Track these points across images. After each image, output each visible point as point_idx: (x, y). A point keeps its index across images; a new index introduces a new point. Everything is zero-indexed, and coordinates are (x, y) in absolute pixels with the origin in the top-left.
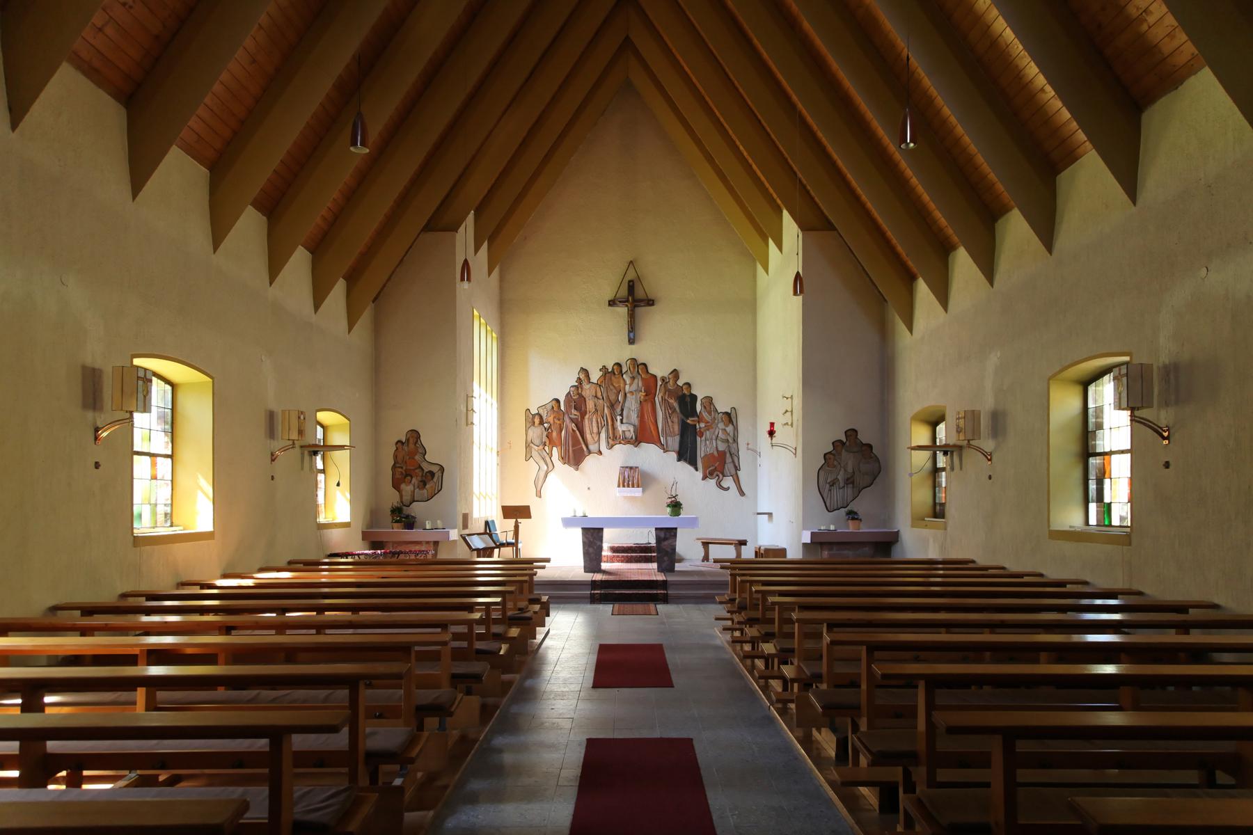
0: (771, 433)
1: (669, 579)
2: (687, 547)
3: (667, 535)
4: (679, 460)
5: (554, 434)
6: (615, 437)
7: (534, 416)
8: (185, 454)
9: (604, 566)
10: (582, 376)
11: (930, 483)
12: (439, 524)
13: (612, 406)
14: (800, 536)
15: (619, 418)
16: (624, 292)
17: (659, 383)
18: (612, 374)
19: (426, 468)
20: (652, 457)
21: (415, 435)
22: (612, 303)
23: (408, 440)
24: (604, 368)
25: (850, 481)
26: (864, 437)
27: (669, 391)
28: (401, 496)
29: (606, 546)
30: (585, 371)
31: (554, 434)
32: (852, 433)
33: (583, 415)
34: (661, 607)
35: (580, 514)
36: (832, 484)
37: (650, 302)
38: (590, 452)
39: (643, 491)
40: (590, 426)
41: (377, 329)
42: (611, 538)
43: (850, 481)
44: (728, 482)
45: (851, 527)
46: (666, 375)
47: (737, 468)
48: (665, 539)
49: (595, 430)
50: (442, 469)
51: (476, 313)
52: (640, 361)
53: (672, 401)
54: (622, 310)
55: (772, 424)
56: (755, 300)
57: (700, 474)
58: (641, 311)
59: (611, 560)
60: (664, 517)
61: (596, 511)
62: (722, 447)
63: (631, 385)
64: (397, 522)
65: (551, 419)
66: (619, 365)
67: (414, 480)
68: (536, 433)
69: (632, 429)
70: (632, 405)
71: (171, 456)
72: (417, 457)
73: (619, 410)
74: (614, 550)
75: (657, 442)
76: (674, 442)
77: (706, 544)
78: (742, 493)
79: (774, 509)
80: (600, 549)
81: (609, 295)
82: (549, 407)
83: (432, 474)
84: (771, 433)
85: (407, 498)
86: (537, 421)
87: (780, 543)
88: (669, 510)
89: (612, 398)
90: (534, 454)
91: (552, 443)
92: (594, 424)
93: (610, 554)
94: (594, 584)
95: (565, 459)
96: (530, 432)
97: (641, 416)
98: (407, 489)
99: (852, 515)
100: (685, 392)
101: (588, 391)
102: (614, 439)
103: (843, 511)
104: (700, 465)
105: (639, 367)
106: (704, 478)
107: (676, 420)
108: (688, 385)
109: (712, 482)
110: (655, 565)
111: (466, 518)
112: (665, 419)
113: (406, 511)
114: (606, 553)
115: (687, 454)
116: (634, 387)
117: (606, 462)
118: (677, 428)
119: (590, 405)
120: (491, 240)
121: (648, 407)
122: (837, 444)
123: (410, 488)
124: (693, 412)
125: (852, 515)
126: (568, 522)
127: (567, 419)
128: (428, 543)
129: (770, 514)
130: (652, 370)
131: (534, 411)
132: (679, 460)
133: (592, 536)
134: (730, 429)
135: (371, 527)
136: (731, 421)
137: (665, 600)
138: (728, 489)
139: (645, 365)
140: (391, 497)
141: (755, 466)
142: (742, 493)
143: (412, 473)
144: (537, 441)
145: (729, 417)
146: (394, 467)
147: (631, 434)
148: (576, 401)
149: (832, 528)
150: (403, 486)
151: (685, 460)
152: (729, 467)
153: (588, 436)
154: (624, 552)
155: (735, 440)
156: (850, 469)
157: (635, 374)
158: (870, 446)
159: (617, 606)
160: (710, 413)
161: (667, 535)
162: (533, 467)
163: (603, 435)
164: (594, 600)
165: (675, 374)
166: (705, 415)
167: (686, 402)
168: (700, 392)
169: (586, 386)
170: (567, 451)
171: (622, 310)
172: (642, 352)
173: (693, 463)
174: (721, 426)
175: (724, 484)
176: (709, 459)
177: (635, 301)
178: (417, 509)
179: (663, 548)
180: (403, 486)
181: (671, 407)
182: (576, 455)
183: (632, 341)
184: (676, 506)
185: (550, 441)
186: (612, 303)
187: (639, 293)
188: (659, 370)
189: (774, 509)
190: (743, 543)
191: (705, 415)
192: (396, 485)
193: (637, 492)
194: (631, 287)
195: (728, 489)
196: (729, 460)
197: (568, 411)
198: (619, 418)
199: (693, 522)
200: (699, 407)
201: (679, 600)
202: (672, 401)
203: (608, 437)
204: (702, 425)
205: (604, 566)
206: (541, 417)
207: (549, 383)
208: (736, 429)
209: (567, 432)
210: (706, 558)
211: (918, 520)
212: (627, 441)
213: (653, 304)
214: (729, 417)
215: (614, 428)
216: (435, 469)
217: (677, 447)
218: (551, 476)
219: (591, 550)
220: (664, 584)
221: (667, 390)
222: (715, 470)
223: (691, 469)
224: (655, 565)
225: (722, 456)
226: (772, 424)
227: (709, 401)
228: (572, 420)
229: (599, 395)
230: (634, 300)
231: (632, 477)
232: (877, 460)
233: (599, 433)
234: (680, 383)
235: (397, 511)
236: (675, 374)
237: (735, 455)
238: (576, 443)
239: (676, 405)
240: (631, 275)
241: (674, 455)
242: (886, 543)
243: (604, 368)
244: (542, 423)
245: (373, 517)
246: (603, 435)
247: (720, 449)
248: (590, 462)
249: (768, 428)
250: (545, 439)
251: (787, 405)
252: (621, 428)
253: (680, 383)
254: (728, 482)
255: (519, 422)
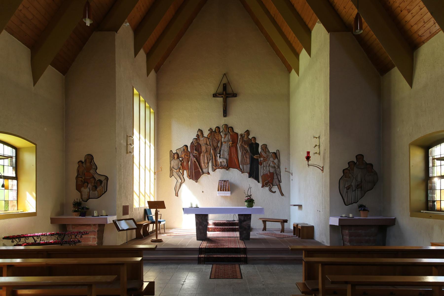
0: (308, 158)
1: (248, 247)
2: (256, 223)
3: (245, 219)
4: (250, 177)
5: (185, 163)
6: (216, 165)
7: (174, 154)
8: (22, 178)
9: (210, 234)
10: (199, 134)
11: (423, 187)
12: (104, 212)
13: (215, 149)
14: (328, 220)
15: (218, 155)
16: (221, 90)
17: (239, 137)
18: (214, 132)
19: (97, 178)
20: (235, 176)
21: (90, 158)
22: (215, 95)
23: (86, 160)
24: (211, 130)
25: (359, 186)
26: (367, 160)
27: (244, 141)
28: (82, 195)
29: (210, 222)
30: (200, 131)
31: (185, 163)
32: (360, 157)
33: (200, 153)
34: (243, 267)
35: (194, 206)
36: (348, 188)
37: (235, 95)
38: (203, 173)
39: (231, 193)
40: (203, 159)
41: (67, 90)
42: (212, 219)
43: (359, 186)
44: (275, 188)
45: (362, 216)
46: (243, 133)
47: (280, 182)
48: (244, 221)
49: (206, 161)
50: (107, 178)
51: (135, 91)
52: (230, 126)
53: (246, 146)
54: (220, 100)
55: (308, 153)
56: (289, 94)
57: (260, 185)
58: (229, 99)
59: (214, 230)
60: (243, 207)
61: (202, 204)
62: (272, 170)
63: (224, 138)
64: (75, 211)
65: (183, 156)
66: (218, 127)
67: (89, 185)
68: (175, 163)
69: (225, 161)
70: (225, 148)
71: (16, 178)
72: (91, 171)
73: (218, 151)
74: (215, 224)
75: (238, 168)
76: (247, 168)
77: (264, 222)
78: (282, 194)
79: (307, 201)
80: (207, 224)
81: (213, 91)
82: (182, 149)
83: (101, 182)
84: (308, 158)
85: (85, 196)
86: (176, 157)
87: (310, 222)
88: (246, 203)
89: (215, 144)
90: (175, 174)
91: (184, 168)
92: (206, 158)
93: (213, 226)
94: (201, 250)
95: (191, 177)
96: (172, 162)
97: (230, 154)
98: (85, 191)
99: (362, 208)
100: (253, 141)
101: (202, 141)
102: (216, 166)
103: (356, 205)
104: (260, 180)
105: (229, 129)
106: (263, 187)
107: (248, 156)
108: (254, 138)
109: (267, 189)
110: (237, 234)
111: (126, 210)
112: (242, 156)
113: (84, 204)
114: (211, 226)
115: (254, 174)
116: (226, 139)
117: (212, 178)
118: (248, 160)
119: (203, 148)
120: (157, 70)
121: (233, 149)
122: (351, 164)
123: (87, 190)
124: (257, 152)
125: (362, 208)
126: (186, 211)
127: (191, 154)
128: (94, 225)
129: (300, 206)
130: (236, 130)
131: (174, 152)
132: (250, 177)
133: (202, 220)
134: (276, 161)
135: (62, 214)
136: (276, 157)
137: (245, 261)
138: (275, 192)
139: (232, 128)
140: (75, 196)
141: (289, 180)
142: (282, 194)
143: (84, 182)
144: (176, 167)
145: (276, 155)
146: (77, 178)
147: (225, 163)
148: (196, 145)
149: (351, 215)
150: (82, 189)
151: (253, 177)
152: (275, 181)
153: (203, 165)
154: (220, 226)
155: (279, 167)
156: (359, 180)
157: (227, 132)
158: (371, 165)
159: (214, 266)
160: (266, 153)
161: (245, 219)
162: (174, 181)
163: (210, 164)
164: (200, 261)
165: (248, 132)
166: (263, 154)
167: (253, 146)
168: (260, 142)
169: (201, 139)
170: (191, 172)
171: (220, 100)
172: (231, 121)
173: (257, 179)
174: (271, 159)
175: (273, 190)
176: (265, 176)
177: (226, 94)
178: (92, 203)
179: (243, 224)
180: (82, 189)
181: (245, 149)
182: (196, 175)
183: (225, 114)
184: (250, 202)
185: (182, 167)
186: (215, 95)
187: (229, 90)
188: (239, 130)
189: (307, 201)
190: (286, 221)
191: (263, 154)
192: (78, 188)
193: (228, 194)
194: (225, 87)
195: (275, 192)
196: (275, 177)
197: (192, 152)
198: (218, 155)
199: (261, 211)
200: (260, 150)
201: (255, 261)
202: (246, 146)
203: (213, 165)
204: (262, 159)
205: (210, 234)
206: (178, 155)
207: (182, 137)
208: (279, 161)
209: (191, 163)
210: (265, 229)
211: (415, 212)
212: (222, 167)
213: (236, 96)
214: (276, 155)
215: (216, 161)
216: (102, 178)
217: (248, 171)
218: (184, 185)
219: (201, 227)
220: (244, 251)
221: (243, 141)
222: (268, 182)
223: (256, 182)
224: (237, 234)
225: (272, 175)
226: (308, 153)
227: (265, 147)
228: (194, 156)
229: (208, 143)
230: (226, 94)
231: (224, 186)
232: (376, 174)
233: (208, 163)
234: (250, 137)
235: (77, 205)
236: (248, 132)
237: (278, 175)
238: (196, 168)
239: (248, 148)
240: (225, 81)
241: (247, 175)
242: (386, 226)
243: (211, 130)
244: (178, 157)
245: (61, 209)
246: (210, 164)
247: (271, 171)
248: (203, 178)
249: (306, 155)
250: (180, 166)
251: (316, 141)
252: (219, 160)
253: (250, 137)
254: (275, 188)
255: (167, 157)
